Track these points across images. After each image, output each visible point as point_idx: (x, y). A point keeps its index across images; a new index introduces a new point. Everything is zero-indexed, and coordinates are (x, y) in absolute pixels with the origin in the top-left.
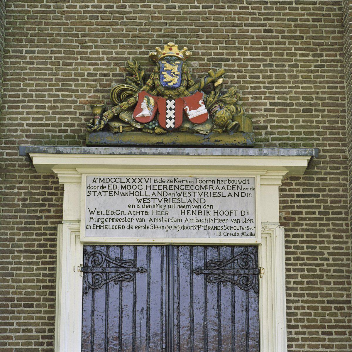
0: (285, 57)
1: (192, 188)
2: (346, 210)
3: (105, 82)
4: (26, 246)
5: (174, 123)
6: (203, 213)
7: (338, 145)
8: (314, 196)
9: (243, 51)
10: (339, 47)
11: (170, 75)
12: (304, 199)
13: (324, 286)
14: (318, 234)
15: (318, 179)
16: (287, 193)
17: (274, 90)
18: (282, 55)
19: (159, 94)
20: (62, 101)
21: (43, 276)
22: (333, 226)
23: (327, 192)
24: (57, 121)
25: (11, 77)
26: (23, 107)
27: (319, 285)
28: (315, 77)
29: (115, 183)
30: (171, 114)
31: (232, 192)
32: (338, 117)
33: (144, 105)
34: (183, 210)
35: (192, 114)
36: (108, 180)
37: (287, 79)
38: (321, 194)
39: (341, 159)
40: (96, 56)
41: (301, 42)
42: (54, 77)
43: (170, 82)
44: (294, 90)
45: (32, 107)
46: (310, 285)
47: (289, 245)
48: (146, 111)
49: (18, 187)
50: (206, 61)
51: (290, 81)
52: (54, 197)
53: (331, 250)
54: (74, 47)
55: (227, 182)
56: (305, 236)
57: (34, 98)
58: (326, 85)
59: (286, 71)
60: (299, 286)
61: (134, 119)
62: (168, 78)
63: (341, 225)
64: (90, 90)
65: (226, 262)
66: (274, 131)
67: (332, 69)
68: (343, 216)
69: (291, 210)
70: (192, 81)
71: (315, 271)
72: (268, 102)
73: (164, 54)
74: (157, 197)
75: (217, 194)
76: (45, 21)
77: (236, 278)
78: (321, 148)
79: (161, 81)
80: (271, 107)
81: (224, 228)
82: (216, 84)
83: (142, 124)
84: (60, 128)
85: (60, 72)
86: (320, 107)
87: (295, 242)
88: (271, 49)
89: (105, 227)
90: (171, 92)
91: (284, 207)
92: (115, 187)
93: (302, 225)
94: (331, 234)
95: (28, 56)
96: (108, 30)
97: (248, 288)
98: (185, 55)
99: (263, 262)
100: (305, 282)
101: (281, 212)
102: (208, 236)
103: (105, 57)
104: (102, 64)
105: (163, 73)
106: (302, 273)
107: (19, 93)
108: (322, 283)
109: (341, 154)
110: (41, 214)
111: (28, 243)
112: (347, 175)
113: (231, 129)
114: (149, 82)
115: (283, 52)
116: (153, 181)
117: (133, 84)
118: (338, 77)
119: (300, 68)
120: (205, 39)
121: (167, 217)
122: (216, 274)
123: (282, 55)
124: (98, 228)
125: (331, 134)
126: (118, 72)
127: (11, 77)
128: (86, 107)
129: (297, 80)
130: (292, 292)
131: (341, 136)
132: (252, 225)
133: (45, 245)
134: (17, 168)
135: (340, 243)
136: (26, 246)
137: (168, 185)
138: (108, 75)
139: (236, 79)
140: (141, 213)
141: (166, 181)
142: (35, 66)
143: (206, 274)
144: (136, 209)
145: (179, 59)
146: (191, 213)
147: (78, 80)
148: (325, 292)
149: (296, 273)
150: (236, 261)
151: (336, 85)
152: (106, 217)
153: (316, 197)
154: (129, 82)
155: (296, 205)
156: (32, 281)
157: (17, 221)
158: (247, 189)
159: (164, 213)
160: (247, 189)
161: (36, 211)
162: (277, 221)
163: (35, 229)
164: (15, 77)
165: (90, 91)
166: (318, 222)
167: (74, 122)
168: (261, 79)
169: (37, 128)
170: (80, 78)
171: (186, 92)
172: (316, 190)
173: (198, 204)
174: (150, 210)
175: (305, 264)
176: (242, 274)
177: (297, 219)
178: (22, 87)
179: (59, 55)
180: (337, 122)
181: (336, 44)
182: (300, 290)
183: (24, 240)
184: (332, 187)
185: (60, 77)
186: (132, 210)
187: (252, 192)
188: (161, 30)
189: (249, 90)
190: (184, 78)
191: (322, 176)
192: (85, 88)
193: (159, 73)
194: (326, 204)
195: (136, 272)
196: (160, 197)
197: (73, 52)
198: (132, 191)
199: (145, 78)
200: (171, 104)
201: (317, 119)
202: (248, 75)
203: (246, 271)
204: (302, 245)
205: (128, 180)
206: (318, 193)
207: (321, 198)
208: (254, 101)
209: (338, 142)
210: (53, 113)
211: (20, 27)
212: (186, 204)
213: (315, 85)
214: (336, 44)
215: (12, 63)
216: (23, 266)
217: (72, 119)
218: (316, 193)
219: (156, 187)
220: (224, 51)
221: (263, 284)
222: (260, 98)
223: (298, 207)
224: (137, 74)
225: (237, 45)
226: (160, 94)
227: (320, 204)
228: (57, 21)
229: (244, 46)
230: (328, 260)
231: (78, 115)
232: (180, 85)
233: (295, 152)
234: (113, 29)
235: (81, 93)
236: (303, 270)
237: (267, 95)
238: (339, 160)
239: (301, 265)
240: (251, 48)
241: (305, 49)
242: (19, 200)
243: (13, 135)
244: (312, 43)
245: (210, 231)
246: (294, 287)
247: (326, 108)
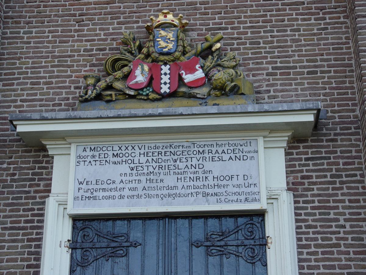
0: (286, 22)
1: (189, 153)
2: (361, 172)
3: (101, 56)
4: (11, 222)
5: (169, 88)
6: (201, 179)
7: (348, 105)
8: (325, 158)
9: (243, 19)
10: (342, 9)
11: (165, 41)
12: (313, 162)
13: (343, 257)
14: (331, 199)
15: (327, 141)
16: (295, 156)
17: (276, 54)
18: (283, 21)
19: (155, 61)
20: (58, 77)
21: (28, 254)
22: (347, 189)
23: (339, 154)
24: (51, 96)
25: (8, 56)
26: (18, 84)
27: (336, 256)
28: (318, 40)
29: (106, 152)
30: (165, 79)
31: (233, 156)
32: (346, 77)
33: (138, 72)
34: (179, 176)
35: (188, 78)
36: (99, 149)
37: (289, 43)
38: (332, 156)
39: (352, 119)
40: (93, 33)
41: (302, 8)
42: (50, 55)
43: (166, 47)
44: (296, 54)
45: (27, 83)
46: (326, 256)
47: (300, 224)
48: (140, 77)
49: (8, 162)
50: (204, 31)
51: (292, 45)
52: (44, 171)
53: (348, 216)
54: (71, 25)
55: (227, 146)
56: (316, 201)
57: (29, 75)
58: (331, 47)
59: (287, 36)
60: (313, 257)
61: (128, 87)
62: (163, 44)
63: (357, 188)
64: (86, 65)
65: (229, 232)
66: (278, 94)
67: (336, 30)
68: (359, 178)
69: (299, 175)
70: (188, 47)
71: (331, 239)
72: (270, 66)
73: (159, 22)
74: (151, 164)
75: (216, 159)
76: (44, 3)
77: (240, 249)
78: (329, 109)
79: (156, 48)
80: (273, 71)
81: (224, 193)
82: (214, 49)
83: (135, 90)
84: (53, 103)
85: (57, 49)
86: (326, 69)
87: (306, 208)
88: (271, 16)
89: (95, 198)
90: (166, 58)
91: (292, 172)
92: (106, 156)
93: (313, 189)
94: (346, 198)
95: (26, 36)
96: (106, 8)
97: (254, 261)
98: (181, 22)
99: (270, 230)
100: (320, 253)
101: (289, 176)
102: (207, 204)
103: (102, 33)
104: (99, 40)
105: (158, 40)
106: (315, 242)
107: (14, 71)
108: (339, 253)
109: (351, 114)
110: (30, 189)
111: (14, 219)
112: (360, 135)
113: (230, 90)
114: (145, 50)
115: (284, 18)
116: (146, 148)
117: (127, 54)
118: (344, 38)
119: (302, 32)
120: (203, 11)
121: (161, 184)
122: (218, 246)
123: (283, 21)
124: (87, 199)
125: (339, 94)
126: (115, 46)
127: (8, 56)
128: (81, 81)
129: (299, 43)
130: (305, 264)
131: (350, 96)
132: (256, 190)
133: (32, 221)
134: (8, 143)
135: (358, 208)
136: (11, 222)
137: (163, 151)
138: (104, 49)
139: (235, 46)
140: (134, 182)
141: (161, 147)
142: (32, 45)
143: (207, 246)
144: (128, 178)
145: (175, 26)
146: (188, 179)
147: (74, 56)
148: (344, 263)
149: (309, 243)
150: (240, 231)
151: (341, 46)
152: (96, 187)
153: (326, 159)
154: (124, 52)
155: (305, 168)
156: (16, 260)
157: (4, 197)
158: (249, 152)
159: (159, 181)
160: (249, 152)
161: (24, 186)
162: (285, 186)
163: (22, 205)
164: (12, 56)
165: (85, 66)
166: (331, 186)
167: (69, 96)
168: (262, 45)
169: (31, 103)
170: (76, 54)
171: (182, 58)
172: (326, 152)
173: (195, 170)
174: (143, 178)
175: (318, 233)
176: (247, 245)
177: (306, 184)
178: (18, 65)
179: (57, 34)
180: (345, 82)
181: (339, 6)
182: (315, 262)
183: (10, 217)
184: (344, 149)
185: (56, 54)
186: (124, 178)
187: (254, 155)
188: (159, 5)
189: (250, 56)
190: (179, 44)
191: (332, 137)
192: (81, 63)
193: (154, 41)
194: (339, 167)
195: (128, 246)
196: (154, 164)
197: (70, 31)
198: (124, 159)
199: (140, 48)
200: (165, 69)
201: (322, 80)
202: (248, 41)
203: (252, 242)
204: (314, 211)
205: (120, 148)
206: (329, 155)
207: (332, 160)
208: (256, 66)
209: (348, 102)
210: (47, 88)
211: (19, 11)
212: (182, 171)
213: (320, 47)
214: (339, 6)
215: (9, 43)
216: (7, 245)
217: (67, 93)
218: (326, 155)
219: (150, 154)
220: (222, 21)
221: (271, 254)
222: (262, 63)
223: (307, 171)
224: (132, 44)
225: (236, 14)
226: (155, 62)
227: (331, 167)
228: (55, 3)
229: (243, 15)
230: (344, 227)
231: (72, 89)
232: (176, 51)
233: (299, 106)
234: (111, 8)
235: (77, 68)
236: (316, 239)
237: (269, 59)
238: (350, 120)
239: (314, 233)
240: (251, 16)
241: (306, 14)
242: (7, 175)
243: (6, 111)
244: (313, 8)
245: (209, 197)
246: (307, 259)
247: (332, 69)
